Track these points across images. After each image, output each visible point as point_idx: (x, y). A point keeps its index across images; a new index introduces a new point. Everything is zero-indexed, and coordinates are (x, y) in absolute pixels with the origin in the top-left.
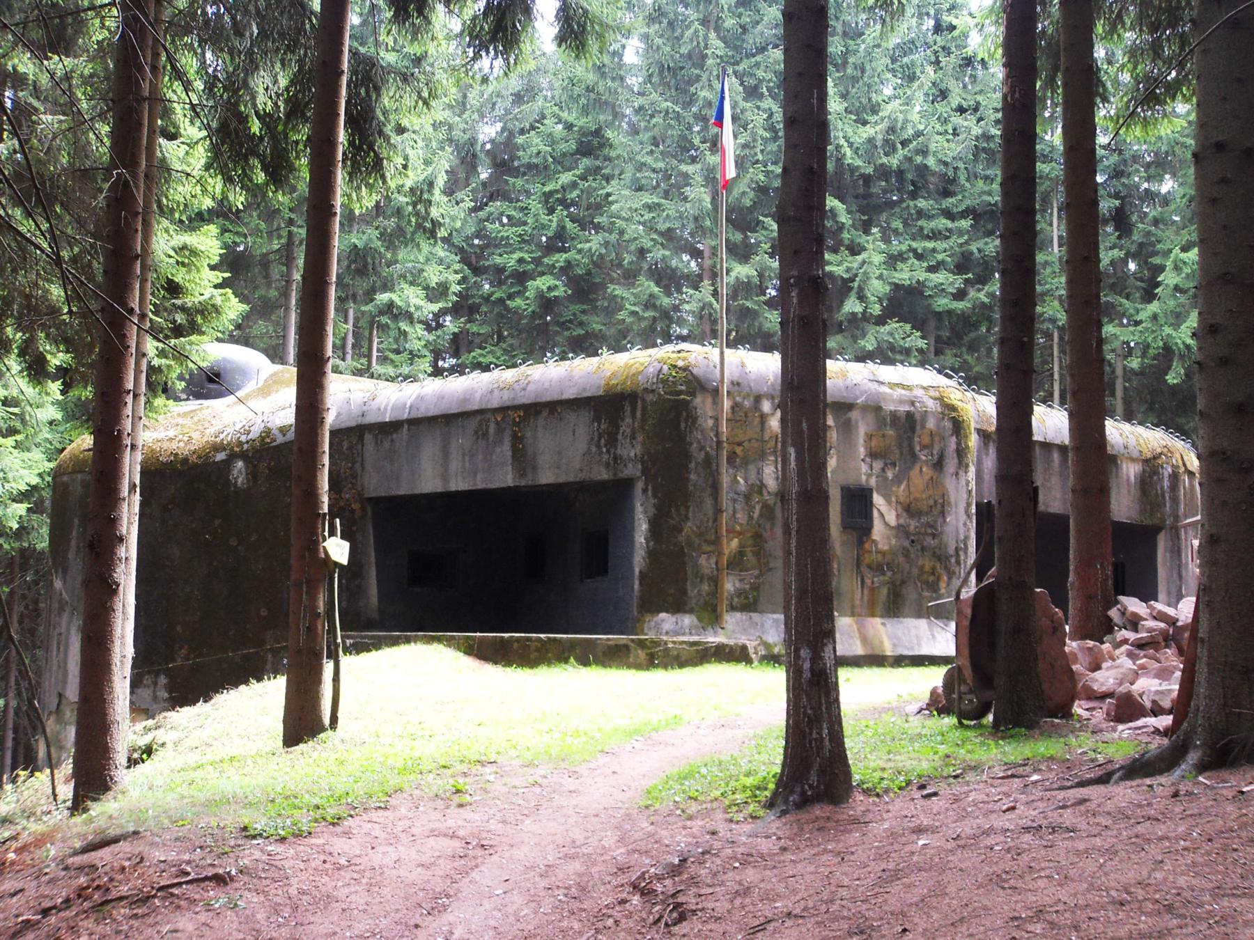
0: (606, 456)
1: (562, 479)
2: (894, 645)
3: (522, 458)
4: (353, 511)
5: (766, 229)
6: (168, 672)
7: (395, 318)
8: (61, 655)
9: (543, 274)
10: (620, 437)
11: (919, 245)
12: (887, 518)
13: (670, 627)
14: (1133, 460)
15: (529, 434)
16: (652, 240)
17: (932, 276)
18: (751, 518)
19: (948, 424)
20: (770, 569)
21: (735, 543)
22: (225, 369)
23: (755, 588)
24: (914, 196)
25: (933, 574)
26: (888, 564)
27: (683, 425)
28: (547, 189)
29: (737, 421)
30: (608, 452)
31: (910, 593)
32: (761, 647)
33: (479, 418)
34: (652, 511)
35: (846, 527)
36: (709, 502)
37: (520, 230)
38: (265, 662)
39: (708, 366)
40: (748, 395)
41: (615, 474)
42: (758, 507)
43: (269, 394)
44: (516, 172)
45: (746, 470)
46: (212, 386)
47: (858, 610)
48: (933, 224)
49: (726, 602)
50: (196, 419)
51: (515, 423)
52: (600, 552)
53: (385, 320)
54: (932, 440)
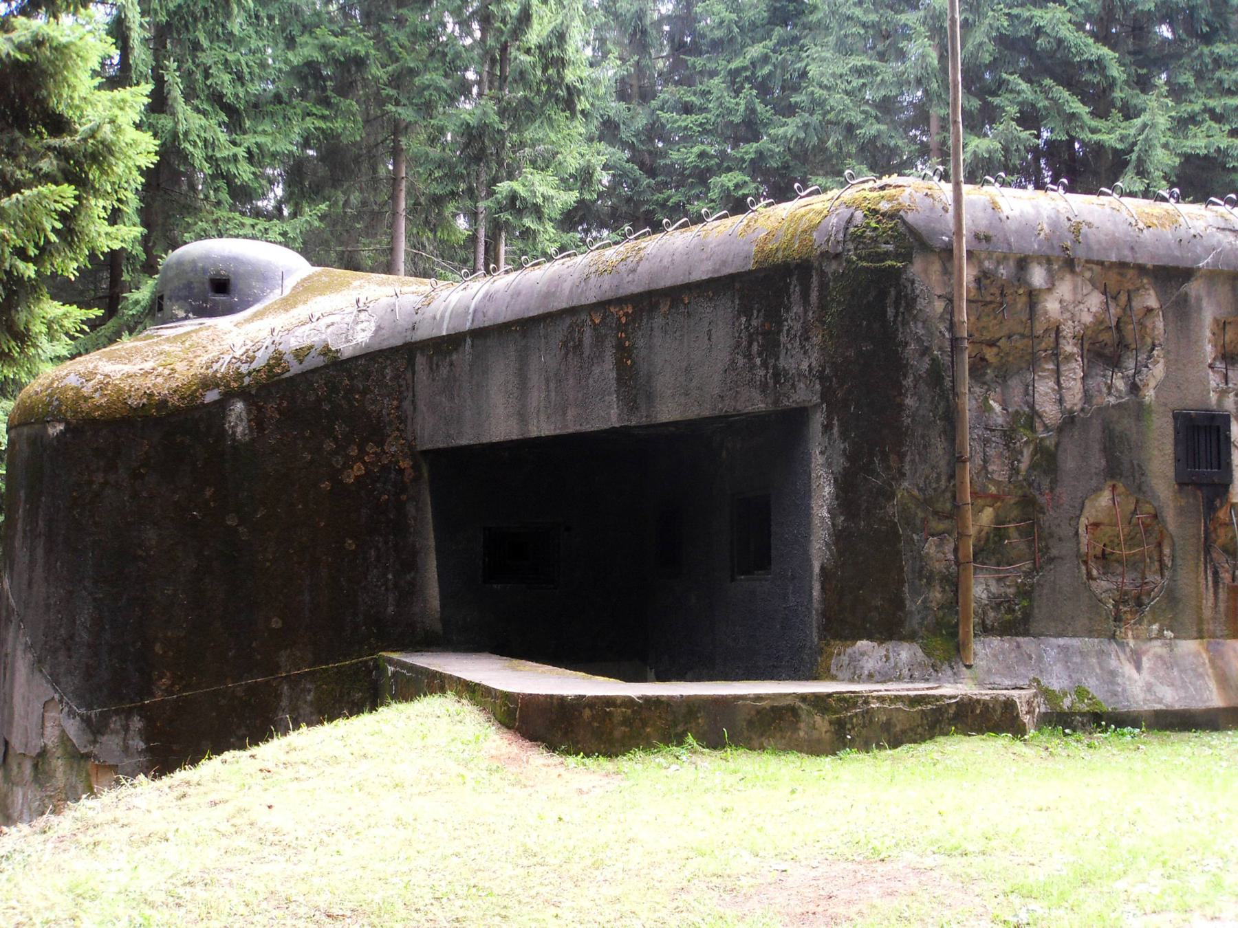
0: (762, 373)
1: (693, 413)
3: (632, 382)
4: (401, 471)
5: (1011, 91)
6: (143, 712)
7: (520, 213)
8: (7, 686)
9: (729, 169)
10: (783, 338)
11: (1216, 103)
13: (876, 673)
15: (641, 343)
18: (1015, 471)
20: (1051, 560)
21: (987, 515)
22: (235, 273)
23: (1025, 593)
24: (1208, 39)
27: (890, 312)
28: (733, 66)
29: (986, 304)
30: (765, 364)
32: (1041, 700)
33: (568, 321)
34: (840, 463)
35: (1183, 482)
36: (939, 447)
37: (701, 118)
38: (278, 697)
39: (932, 209)
40: (1006, 258)
41: (776, 402)
42: (1027, 453)
43: (294, 306)
44: (695, 50)
46: (220, 298)
47: (1209, 627)
50: (187, 344)
51: (621, 327)
52: (758, 533)
53: (505, 216)
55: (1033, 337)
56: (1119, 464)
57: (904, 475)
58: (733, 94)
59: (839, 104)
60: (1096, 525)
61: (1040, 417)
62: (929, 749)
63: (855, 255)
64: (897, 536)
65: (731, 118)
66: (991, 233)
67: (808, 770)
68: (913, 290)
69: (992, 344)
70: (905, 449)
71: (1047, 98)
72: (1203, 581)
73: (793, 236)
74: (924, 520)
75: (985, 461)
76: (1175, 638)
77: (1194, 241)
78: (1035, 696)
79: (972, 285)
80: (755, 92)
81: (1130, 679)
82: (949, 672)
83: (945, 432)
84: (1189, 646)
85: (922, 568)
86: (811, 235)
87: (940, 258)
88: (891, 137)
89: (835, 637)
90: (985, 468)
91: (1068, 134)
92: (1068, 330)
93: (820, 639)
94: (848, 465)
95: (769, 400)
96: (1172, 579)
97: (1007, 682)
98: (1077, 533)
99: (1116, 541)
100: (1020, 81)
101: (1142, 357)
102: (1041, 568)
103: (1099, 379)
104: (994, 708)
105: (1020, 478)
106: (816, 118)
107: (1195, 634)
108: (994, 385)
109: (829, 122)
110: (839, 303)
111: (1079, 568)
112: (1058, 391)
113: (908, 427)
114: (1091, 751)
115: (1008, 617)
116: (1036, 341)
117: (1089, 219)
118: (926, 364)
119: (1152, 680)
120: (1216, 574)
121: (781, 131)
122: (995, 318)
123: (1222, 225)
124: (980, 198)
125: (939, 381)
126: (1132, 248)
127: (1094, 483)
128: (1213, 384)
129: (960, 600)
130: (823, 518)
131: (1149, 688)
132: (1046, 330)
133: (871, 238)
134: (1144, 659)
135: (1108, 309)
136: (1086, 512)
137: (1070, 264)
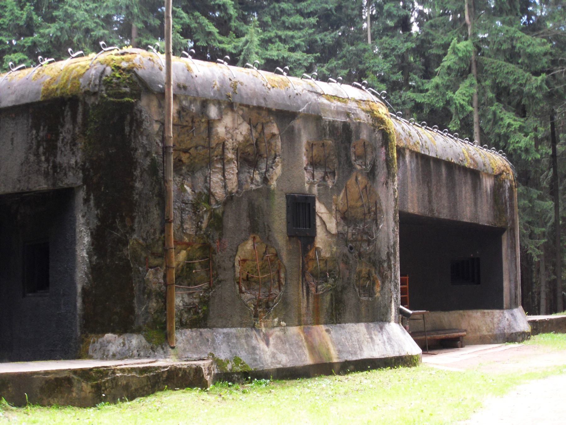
0: (45, 165)
2: (339, 352)
9: (15, 52)
10: (59, 144)
12: (328, 225)
13: (119, 354)
14: (489, 175)
16: (96, 23)
17: (292, 54)
18: (199, 228)
19: (379, 136)
20: (220, 282)
21: (183, 255)
23: (205, 302)
25: (368, 278)
26: (330, 271)
27: (127, 129)
30: (47, 160)
31: (350, 298)
32: (214, 366)
34: (95, 222)
35: (291, 235)
36: (155, 213)
39: (153, 68)
40: (195, 100)
41: (54, 184)
42: (206, 217)
45: (193, 177)
47: (304, 318)
48: (292, 19)
49: (175, 319)
52: (41, 264)
54: (365, 151)
55: (209, 148)
56: (257, 226)
57: (134, 230)
58: (19, 8)
59: (82, 17)
60: (244, 261)
61: (213, 196)
62: (152, 401)
63: (106, 93)
64: (130, 269)
65: (18, 22)
66: (187, 85)
67: (81, 419)
68: (141, 117)
69: (186, 151)
70: (135, 214)
71: (196, 22)
72: (301, 292)
73: (67, 81)
74: (146, 258)
75: (182, 222)
76: (287, 326)
77: (297, 97)
78: (212, 364)
79: (176, 115)
80: (32, 8)
81: (263, 351)
82: (162, 352)
83: (159, 204)
84: (294, 330)
85: (145, 288)
86: (78, 80)
87: (157, 98)
88: (111, 38)
89: (91, 332)
90: (182, 226)
91: (207, 43)
92: (229, 145)
93: (82, 333)
94: (99, 224)
95: (50, 183)
96: (285, 292)
97: (195, 356)
98: (234, 266)
99: (255, 270)
100: (182, 12)
101: (270, 162)
102: (214, 286)
103: (246, 174)
104: (190, 373)
105: (202, 233)
106: (67, 25)
107: (297, 323)
108: (187, 176)
109: (75, 28)
110: (95, 123)
111: (235, 287)
112: (223, 181)
113: (136, 201)
114: (245, 395)
115: (195, 317)
116: (211, 150)
117: (242, 80)
118: (148, 162)
119: (275, 351)
120: (308, 288)
121: (47, 31)
122: (188, 135)
123: (311, 89)
124: (179, 63)
125: (155, 172)
126: (265, 99)
127: (243, 235)
128: (307, 179)
129: (168, 308)
130: (83, 257)
131: (274, 356)
132: (217, 144)
133: (116, 84)
134: (271, 339)
135: (251, 134)
136: (239, 253)
137: (231, 106)
